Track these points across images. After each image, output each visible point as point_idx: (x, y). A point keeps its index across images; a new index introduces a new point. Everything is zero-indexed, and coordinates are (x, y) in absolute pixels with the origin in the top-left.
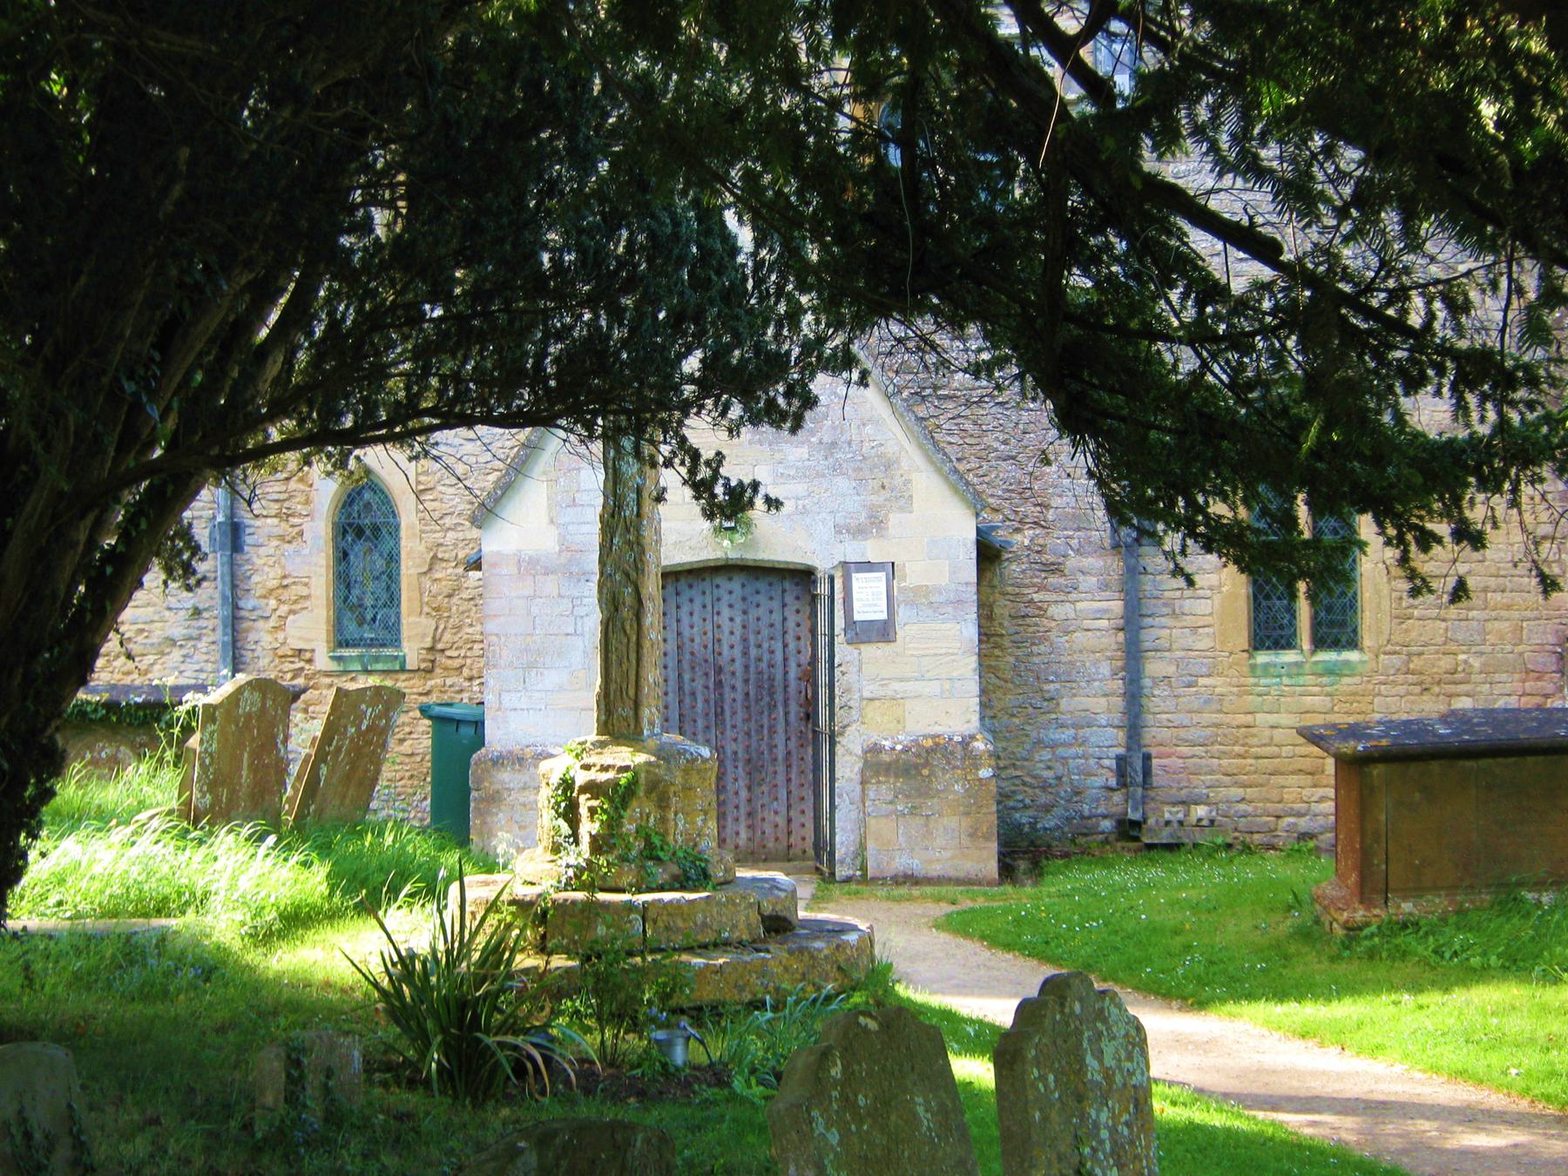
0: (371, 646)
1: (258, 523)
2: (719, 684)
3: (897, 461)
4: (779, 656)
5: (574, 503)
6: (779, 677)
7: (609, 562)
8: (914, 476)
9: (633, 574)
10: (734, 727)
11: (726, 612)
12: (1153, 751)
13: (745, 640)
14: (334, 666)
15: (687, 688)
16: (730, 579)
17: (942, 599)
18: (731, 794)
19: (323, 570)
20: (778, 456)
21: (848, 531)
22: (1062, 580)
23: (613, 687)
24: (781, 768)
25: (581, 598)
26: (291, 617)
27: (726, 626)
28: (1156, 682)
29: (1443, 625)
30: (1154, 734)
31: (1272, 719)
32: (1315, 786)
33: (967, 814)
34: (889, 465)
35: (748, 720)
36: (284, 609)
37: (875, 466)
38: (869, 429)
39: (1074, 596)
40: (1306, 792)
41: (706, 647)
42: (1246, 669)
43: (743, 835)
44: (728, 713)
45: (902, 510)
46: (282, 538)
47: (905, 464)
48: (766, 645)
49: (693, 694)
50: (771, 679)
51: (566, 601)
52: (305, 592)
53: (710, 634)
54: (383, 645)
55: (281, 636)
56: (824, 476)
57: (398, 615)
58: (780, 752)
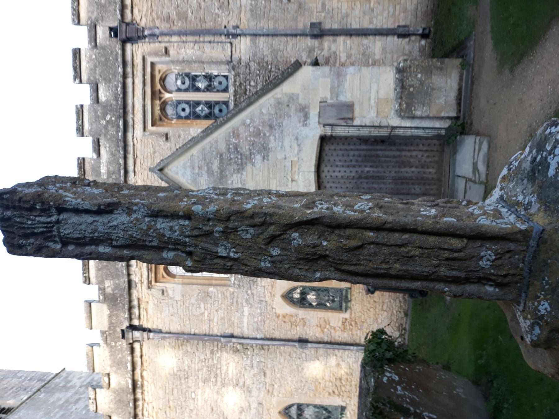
0: (342, 298)
1: (299, 333)
2: (367, 178)
3: (277, 99)
4: (356, 153)
6: (363, 153)
7: (254, 263)
8: (284, 91)
10: (384, 172)
11: (336, 174)
12: (397, 24)
13: (348, 166)
14: (349, 311)
16: (323, 171)
17: (336, 82)
19: (316, 312)
20: (273, 149)
21: (306, 121)
22: (332, 57)
23: (443, 271)
24: (404, 153)
26: (331, 324)
27: (343, 174)
28: (371, 22)
30: (390, 25)
33: (431, 72)
34: (279, 103)
35: (382, 167)
36: (328, 326)
37: (280, 108)
38: (264, 111)
39: (338, 53)
41: (350, 183)
43: (431, 170)
45: (298, 98)
46: (304, 326)
47: (279, 96)
48: (351, 158)
49: (369, 188)
50: (365, 156)
52: (322, 320)
53: (345, 180)
54: (342, 294)
55: (337, 328)
56: (282, 130)
57: (332, 288)
58: (397, 153)
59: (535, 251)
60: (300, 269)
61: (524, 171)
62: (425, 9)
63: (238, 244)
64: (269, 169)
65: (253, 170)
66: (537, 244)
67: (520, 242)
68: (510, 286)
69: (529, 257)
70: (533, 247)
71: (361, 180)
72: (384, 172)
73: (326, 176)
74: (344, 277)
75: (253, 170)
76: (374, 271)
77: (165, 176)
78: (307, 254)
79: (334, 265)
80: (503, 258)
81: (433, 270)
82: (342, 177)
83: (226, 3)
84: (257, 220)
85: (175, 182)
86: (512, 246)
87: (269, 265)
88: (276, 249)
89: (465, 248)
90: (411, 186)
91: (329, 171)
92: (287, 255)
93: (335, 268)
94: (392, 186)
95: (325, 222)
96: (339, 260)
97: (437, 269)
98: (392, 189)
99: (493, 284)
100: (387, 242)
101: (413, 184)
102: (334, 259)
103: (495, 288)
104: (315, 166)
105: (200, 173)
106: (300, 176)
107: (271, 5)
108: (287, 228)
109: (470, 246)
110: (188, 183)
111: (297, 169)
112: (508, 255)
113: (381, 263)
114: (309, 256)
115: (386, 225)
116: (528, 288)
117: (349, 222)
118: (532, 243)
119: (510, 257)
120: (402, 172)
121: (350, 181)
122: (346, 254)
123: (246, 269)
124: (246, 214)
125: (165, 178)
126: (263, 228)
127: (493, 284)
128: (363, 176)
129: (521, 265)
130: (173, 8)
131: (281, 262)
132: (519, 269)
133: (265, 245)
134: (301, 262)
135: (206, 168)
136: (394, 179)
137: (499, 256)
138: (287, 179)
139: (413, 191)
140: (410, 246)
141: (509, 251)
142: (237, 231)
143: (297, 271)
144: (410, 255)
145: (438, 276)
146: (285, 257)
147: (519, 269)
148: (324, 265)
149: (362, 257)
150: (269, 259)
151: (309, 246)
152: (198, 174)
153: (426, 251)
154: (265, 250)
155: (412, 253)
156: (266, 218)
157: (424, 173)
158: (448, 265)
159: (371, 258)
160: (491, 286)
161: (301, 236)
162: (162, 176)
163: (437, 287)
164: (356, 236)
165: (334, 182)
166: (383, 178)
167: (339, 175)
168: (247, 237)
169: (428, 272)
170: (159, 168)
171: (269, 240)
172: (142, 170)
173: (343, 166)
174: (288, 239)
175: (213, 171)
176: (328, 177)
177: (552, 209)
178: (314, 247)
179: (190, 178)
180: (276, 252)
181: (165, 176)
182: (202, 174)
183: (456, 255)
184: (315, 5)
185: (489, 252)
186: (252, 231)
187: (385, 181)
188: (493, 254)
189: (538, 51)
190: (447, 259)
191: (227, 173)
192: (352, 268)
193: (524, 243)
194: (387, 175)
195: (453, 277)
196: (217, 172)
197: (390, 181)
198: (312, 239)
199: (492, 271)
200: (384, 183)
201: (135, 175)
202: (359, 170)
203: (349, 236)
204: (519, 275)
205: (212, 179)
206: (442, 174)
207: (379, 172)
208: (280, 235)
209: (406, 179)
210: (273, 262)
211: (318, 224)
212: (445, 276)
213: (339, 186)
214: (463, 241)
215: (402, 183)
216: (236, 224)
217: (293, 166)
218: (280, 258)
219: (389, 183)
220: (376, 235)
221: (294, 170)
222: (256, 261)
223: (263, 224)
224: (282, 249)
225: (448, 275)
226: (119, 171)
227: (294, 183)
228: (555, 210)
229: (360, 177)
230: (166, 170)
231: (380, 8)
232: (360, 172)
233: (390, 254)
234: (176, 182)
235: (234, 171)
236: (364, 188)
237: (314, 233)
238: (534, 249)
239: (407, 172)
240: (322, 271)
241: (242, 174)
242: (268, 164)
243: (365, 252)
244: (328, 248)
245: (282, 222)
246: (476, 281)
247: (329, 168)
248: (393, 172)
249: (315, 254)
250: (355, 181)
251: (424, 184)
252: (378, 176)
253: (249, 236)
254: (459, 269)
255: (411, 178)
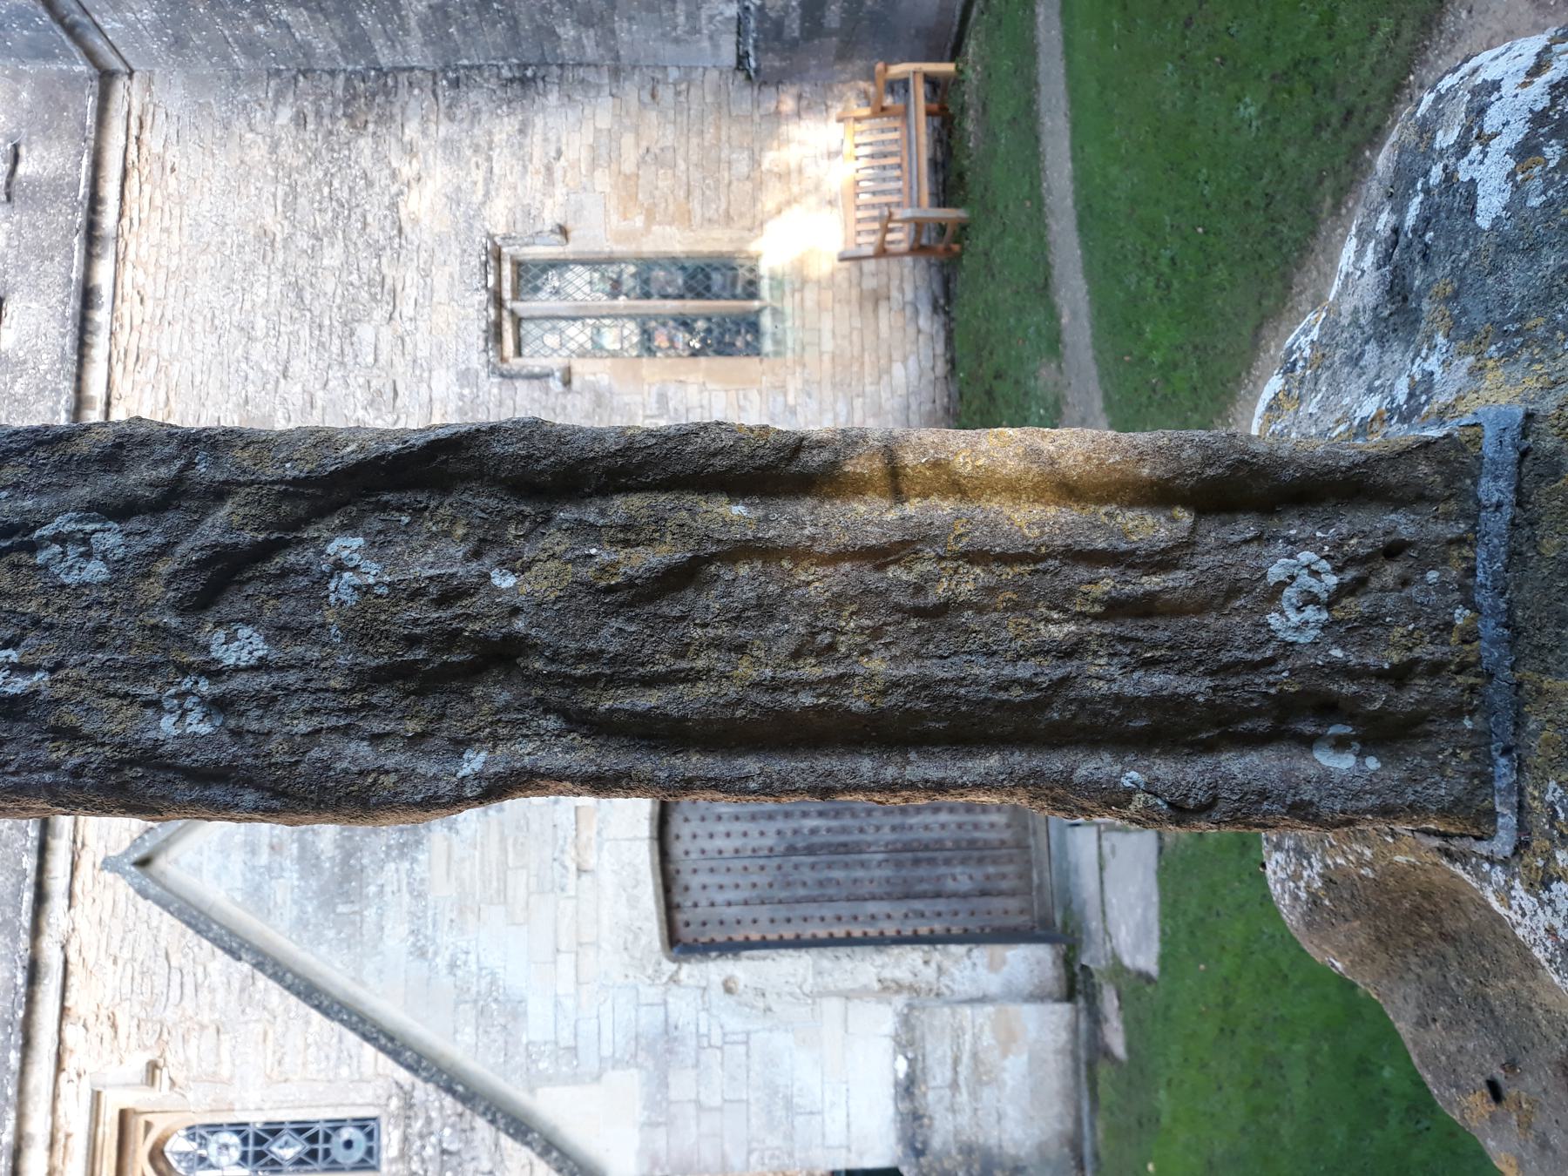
2: (810, 850)
5: (573, 1050)
7: (114, 722)
9: (220, 525)
10: (861, 830)
11: (720, 842)
15: (816, 892)
16: (678, 837)
18: (944, 834)
23: (1104, 676)
25: (698, 1035)
27: (737, 842)
29: (735, 183)
31: (827, 335)
32: (888, 298)
40: (895, 306)
41: (762, 868)
42: (779, 360)
44: (843, 838)
49: (821, 884)
51: (703, 1057)
53: (747, 862)
59: (1514, 525)
60: (376, 739)
61: (1355, 322)
62: (927, 407)
63: (36, 623)
64: (503, 839)
65: (450, 846)
66: (1518, 490)
67: (1434, 500)
68: (1428, 736)
69: (1491, 558)
70: (1499, 505)
71: (795, 859)
72: (861, 830)
73: (687, 853)
74: (613, 760)
75: (450, 846)
76: (765, 699)
77: (157, 882)
78: (412, 641)
79: (556, 695)
80: (1374, 583)
81: (1053, 671)
82: (737, 851)
83: (389, 394)
84: (140, 477)
85: (187, 902)
86: (1403, 525)
87: (205, 729)
88: (245, 632)
89: (1188, 544)
90: (942, 870)
91: (695, 836)
92: (304, 664)
93: (562, 712)
94: (887, 872)
95: (502, 459)
96: (584, 656)
97: (1071, 667)
98: (888, 881)
99: (1347, 730)
100: (813, 538)
101: (947, 862)
102: (552, 660)
103: (1361, 755)
104: (652, 819)
105: (276, 865)
106: (605, 854)
107: (518, 399)
108: (302, 509)
109: (1211, 540)
110: (233, 900)
111: (593, 834)
112: (1391, 572)
113: (796, 655)
114: (420, 654)
115: (804, 456)
116: (1519, 723)
117: (622, 452)
118: (1493, 489)
119: (1405, 582)
120: (911, 828)
121: (762, 862)
122: (616, 623)
123: (75, 760)
124: (83, 447)
125: (154, 890)
126: (172, 518)
127: (1347, 730)
128: (800, 844)
129: (1461, 616)
130: (230, 406)
131: (267, 702)
132: (1454, 638)
133: (181, 608)
134: (380, 696)
135: (295, 846)
136: (893, 849)
137: (1358, 569)
138: (565, 867)
139: (950, 885)
140: (929, 552)
141: (1393, 550)
142: (33, 548)
143: (358, 752)
144: (932, 599)
145: (1083, 703)
146: (292, 678)
147: (1454, 638)
148: (506, 708)
149: (697, 633)
150: (204, 687)
151: (415, 595)
152: (269, 869)
153: (1008, 573)
154: (181, 637)
155: (940, 591)
156: (190, 465)
157: (976, 826)
158: (1124, 640)
159: (742, 633)
160: (1341, 744)
161: (378, 545)
162: (146, 882)
163: (1082, 772)
164: (660, 521)
165: (712, 870)
166: (856, 848)
167: (728, 845)
168: (86, 576)
169: (1028, 685)
170: (136, 856)
171: (203, 578)
172: (98, 888)
173: (737, 818)
174: (306, 572)
175: (318, 858)
176: (693, 856)
177: (1540, 332)
178: (443, 601)
179: (239, 884)
180: (240, 647)
181: (157, 882)
182: (282, 869)
183: (1152, 582)
184: (638, 399)
185: (1306, 556)
186: (110, 538)
187: (865, 857)
188: (1325, 565)
189: (1239, 417)
190: (1115, 608)
191: (365, 861)
192: (648, 700)
193: (1453, 506)
194: (868, 838)
195: (1156, 702)
196: (332, 858)
197: (880, 857)
198: (436, 556)
199: (1337, 653)
200: (863, 864)
201: (70, 907)
202: (788, 826)
203: (625, 528)
204: (1462, 668)
205: (314, 884)
206: (1026, 828)
207: (844, 830)
208: (264, 551)
209: (927, 848)
210: (218, 706)
211: (466, 477)
212: (1118, 699)
213: (726, 880)
214: (1173, 520)
215: (916, 862)
216: (28, 504)
217: (582, 826)
218: (264, 681)
219: (879, 864)
220: (760, 513)
221: (583, 837)
222: (135, 709)
223: (172, 496)
224: (280, 632)
225: (1129, 690)
226: (18, 894)
227: (584, 877)
228: (1553, 331)
229: (791, 850)
230: (161, 863)
231: (814, 405)
232: (789, 834)
233: (837, 602)
234: (192, 899)
235: (387, 854)
236: (804, 884)
237: (447, 534)
238: (1508, 512)
239: (926, 828)
240: (496, 739)
241: (414, 860)
242: (501, 824)
243: (712, 601)
244: (518, 601)
245: (271, 473)
246: (1264, 725)
247: (695, 825)
248: (887, 830)
249: (452, 638)
250: (776, 861)
251: (981, 861)
252: (845, 845)
253: (96, 570)
254: (1175, 658)
255: (939, 845)
